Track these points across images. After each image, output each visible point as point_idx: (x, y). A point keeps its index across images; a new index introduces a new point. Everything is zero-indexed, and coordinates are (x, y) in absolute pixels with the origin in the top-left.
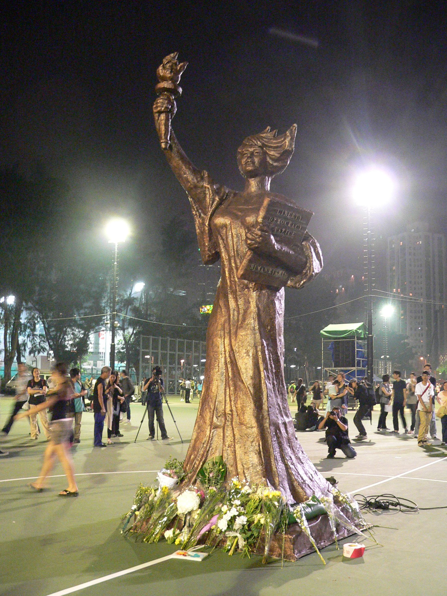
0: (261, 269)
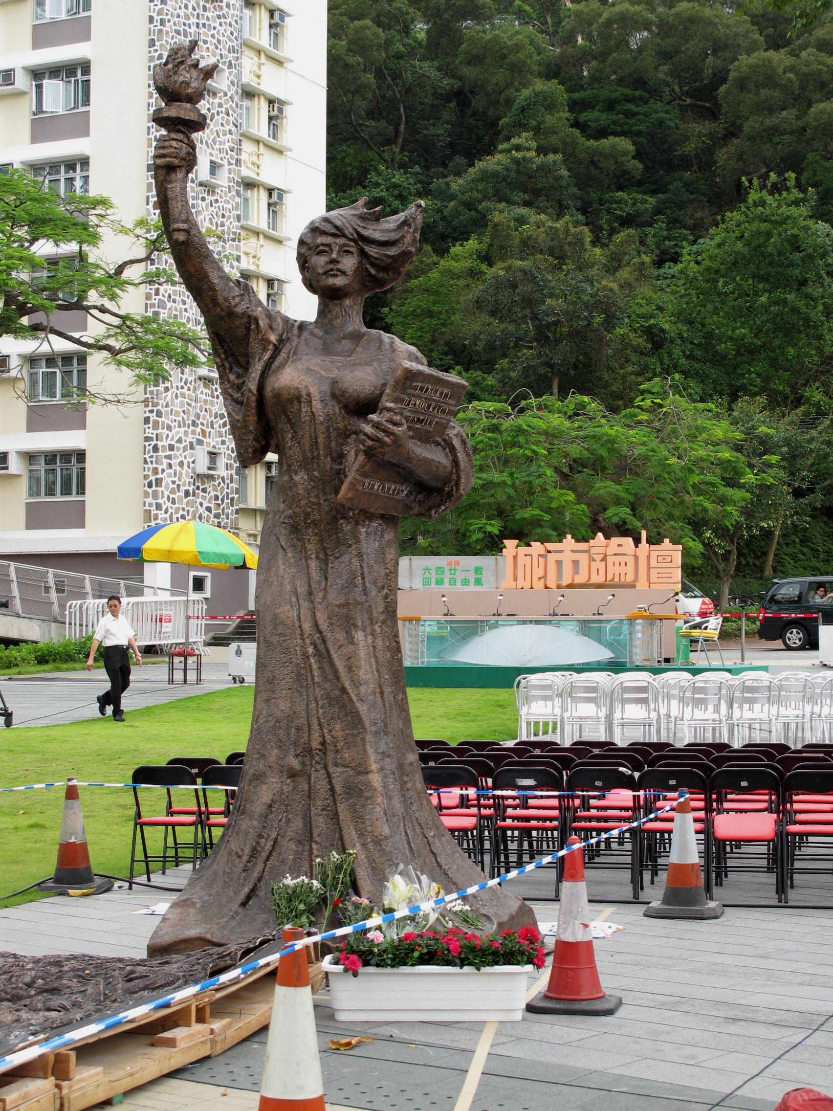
0: (379, 487)
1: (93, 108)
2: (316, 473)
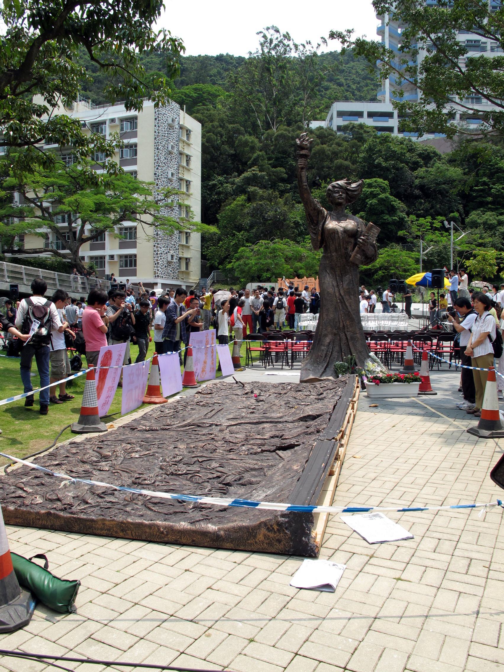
1: (137, 157)
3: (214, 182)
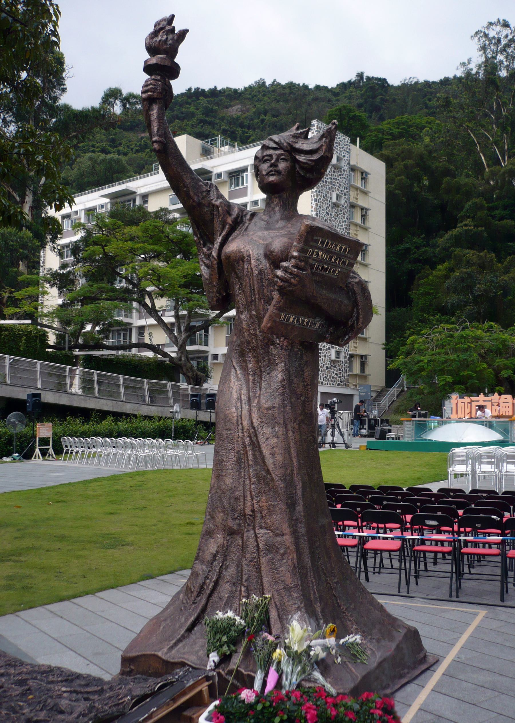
0: (294, 319)
2: (254, 312)
3: (407, 246)
